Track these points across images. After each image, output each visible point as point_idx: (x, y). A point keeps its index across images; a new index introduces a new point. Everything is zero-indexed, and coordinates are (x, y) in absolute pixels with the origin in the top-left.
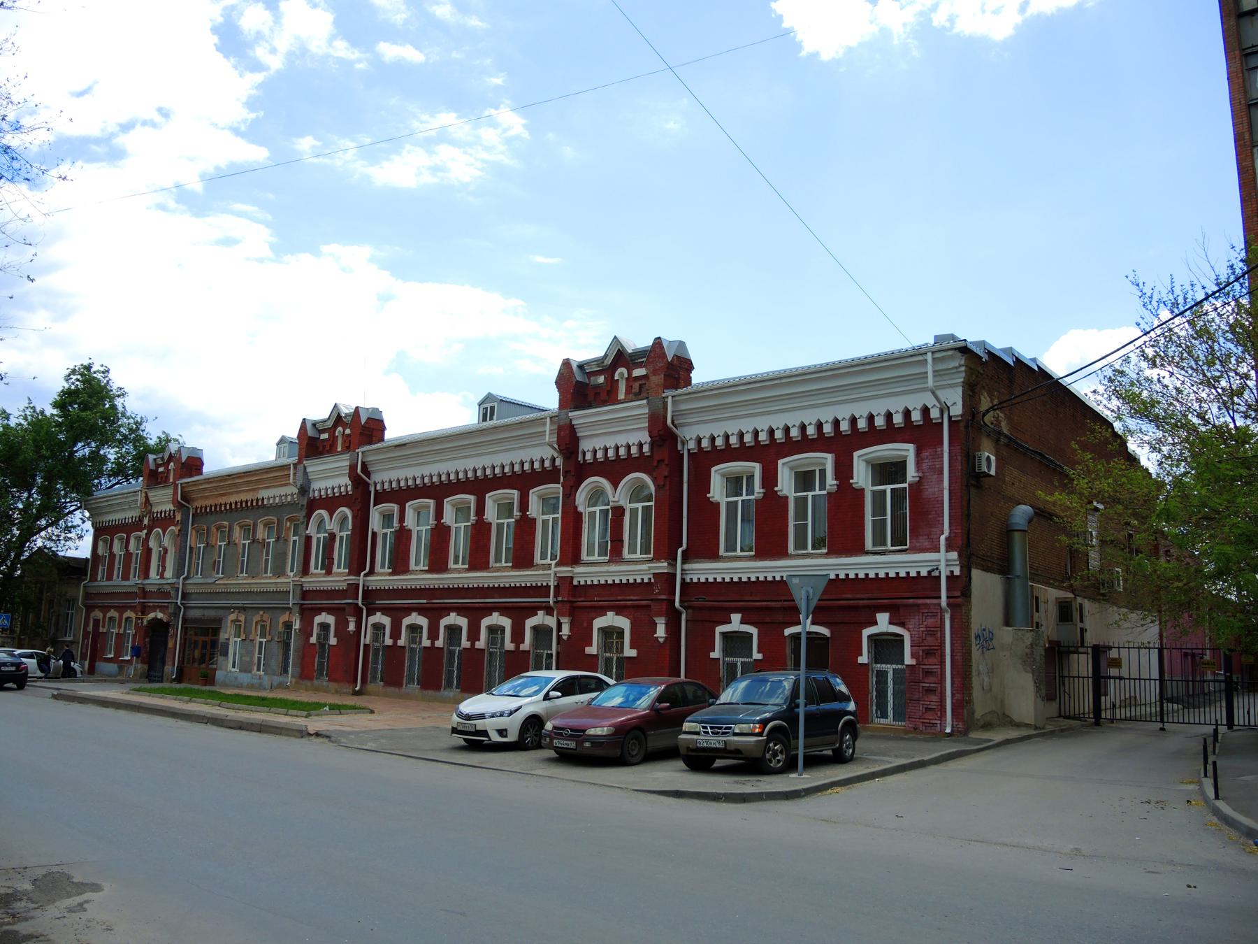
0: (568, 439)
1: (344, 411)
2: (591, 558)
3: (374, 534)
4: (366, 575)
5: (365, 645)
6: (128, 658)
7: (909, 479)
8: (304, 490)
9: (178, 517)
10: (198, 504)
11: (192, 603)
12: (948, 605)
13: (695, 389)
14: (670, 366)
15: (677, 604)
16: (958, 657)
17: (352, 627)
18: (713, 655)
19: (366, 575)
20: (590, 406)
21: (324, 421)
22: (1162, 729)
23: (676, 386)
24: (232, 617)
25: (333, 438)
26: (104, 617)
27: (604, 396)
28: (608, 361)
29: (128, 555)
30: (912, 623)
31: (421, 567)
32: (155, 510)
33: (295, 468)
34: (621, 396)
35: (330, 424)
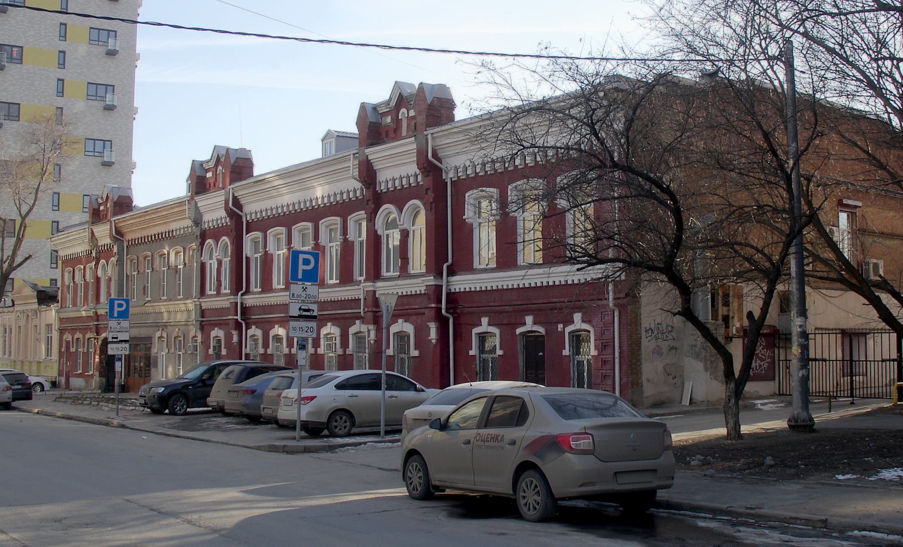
0: (368, 174)
1: (407, 92)
2: (388, 274)
3: (248, 259)
4: (242, 295)
5: (246, 354)
6: (91, 373)
8: (197, 222)
9: (115, 250)
10: (129, 237)
12: (615, 305)
13: (457, 125)
14: (431, 107)
15: (443, 311)
16: (625, 348)
17: (235, 339)
18: (472, 353)
19: (242, 295)
20: (384, 143)
21: (208, 162)
22: (852, 403)
23: (438, 123)
24: (158, 334)
25: (397, 122)
26: (84, 337)
27: (392, 135)
28: (393, 103)
29: (86, 284)
30: (597, 320)
31: (334, 281)
32: (100, 244)
33: (189, 203)
34: (404, 133)
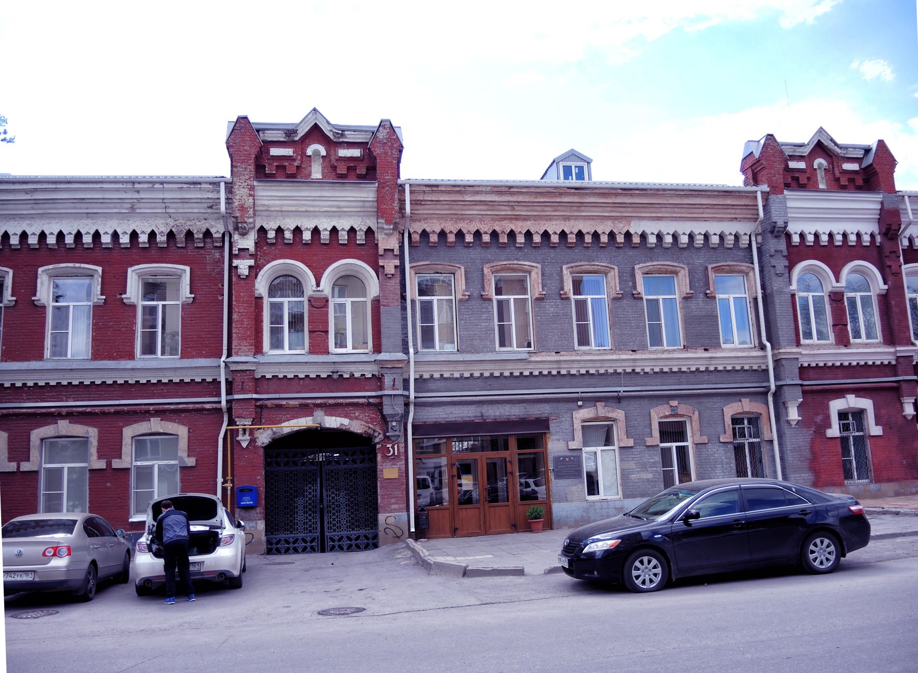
7: (5, 301)
11: (429, 396)
28: (302, 132)
35: (806, 151)
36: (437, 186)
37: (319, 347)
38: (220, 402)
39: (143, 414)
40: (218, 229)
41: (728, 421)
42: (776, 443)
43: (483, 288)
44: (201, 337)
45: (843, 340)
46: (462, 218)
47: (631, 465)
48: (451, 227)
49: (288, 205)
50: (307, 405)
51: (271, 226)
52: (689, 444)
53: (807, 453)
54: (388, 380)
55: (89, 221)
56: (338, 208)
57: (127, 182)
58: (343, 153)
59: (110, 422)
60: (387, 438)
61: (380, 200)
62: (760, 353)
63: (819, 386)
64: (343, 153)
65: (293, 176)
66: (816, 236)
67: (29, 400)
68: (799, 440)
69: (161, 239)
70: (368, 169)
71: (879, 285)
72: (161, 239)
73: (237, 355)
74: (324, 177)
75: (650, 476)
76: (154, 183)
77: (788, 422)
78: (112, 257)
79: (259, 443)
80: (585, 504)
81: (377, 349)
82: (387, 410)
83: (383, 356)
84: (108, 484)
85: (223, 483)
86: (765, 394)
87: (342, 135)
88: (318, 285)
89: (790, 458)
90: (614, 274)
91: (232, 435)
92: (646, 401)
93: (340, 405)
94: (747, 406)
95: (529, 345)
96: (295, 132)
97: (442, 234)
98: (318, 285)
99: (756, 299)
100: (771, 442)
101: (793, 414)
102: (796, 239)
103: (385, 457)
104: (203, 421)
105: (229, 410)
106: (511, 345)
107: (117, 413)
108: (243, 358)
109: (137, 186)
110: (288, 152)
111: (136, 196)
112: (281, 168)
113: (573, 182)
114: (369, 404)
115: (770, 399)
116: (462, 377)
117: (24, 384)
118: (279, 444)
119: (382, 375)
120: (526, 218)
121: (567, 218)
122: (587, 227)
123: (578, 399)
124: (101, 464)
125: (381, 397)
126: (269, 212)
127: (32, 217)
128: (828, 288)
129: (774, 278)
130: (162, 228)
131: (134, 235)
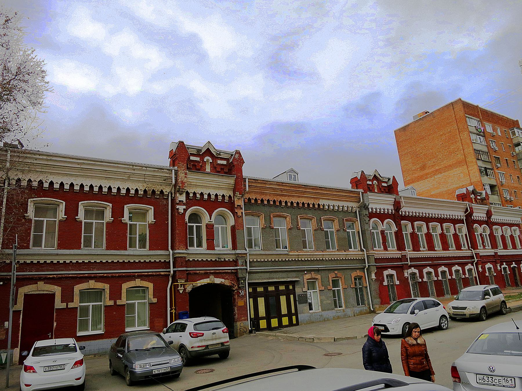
36: (257, 180)
37: (211, 246)
38: (170, 272)
39: (131, 277)
40: (167, 190)
41: (353, 279)
42: (368, 287)
43: (271, 223)
44: (158, 240)
45: (386, 249)
46: (263, 194)
47: (324, 297)
48: (259, 197)
49: (199, 183)
50: (207, 273)
51: (191, 191)
52: (341, 288)
53: (378, 291)
54: (240, 262)
55: (106, 181)
56: (217, 186)
57: (130, 165)
58: (219, 162)
59: (114, 282)
60: (239, 288)
61: (236, 183)
62: (362, 253)
63: (382, 265)
64: (219, 162)
65: (199, 170)
66: (209, 195)
67: (73, 270)
68: (375, 286)
69: (141, 192)
70: (229, 169)
71: (395, 229)
72: (141, 192)
73: (178, 249)
74: (211, 172)
75: (330, 302)
76: (142, 167)
77: (372, 279)
78: (119, 200)
79: (187, 291)
80: (309, 314)
81: (234, 247)
82: (240, 275)
83: (238, 251)
84: (114, 313)
85: (170, 310)
86: (364, 268)
87: (219, 154)
88: (210, 219)
89: (373, 294)
90: (314, 221)
91: (175, 288)
92: (327, 272)
93: (221, 273)
94: (359, 273)
95: (286, 248)
96: (201, 150)
97: (256, 200)
98: (210, 219)
99: (359, 232)
100: (366, 287)
101: (373, 276)
102: (370, 210)
103: (238, 296)
104: (159, 282)
105: (174, 277)
106: (280, 248)
107: (119, 276)
108: (180, 251)
109: (134, 167)
110: (198, 159)
111: (133, 172)
112: (194, 166)
113: (292, 182)
114: (232, 272)
115: (366, 271)
116: (301, 260)
117: (71, 262)
118: (195, 290)
119: (237, 260)
120: (286, 196)
121: (299, 197)
122: (306, 201)
123: (305, 271)
124: (111, 303)
125: (237, 269)
126: (190, 185)
127: (77, 176)
128: (380, 229)
129: (365, 224)
130: (141, 188)
131: (128, 190)
